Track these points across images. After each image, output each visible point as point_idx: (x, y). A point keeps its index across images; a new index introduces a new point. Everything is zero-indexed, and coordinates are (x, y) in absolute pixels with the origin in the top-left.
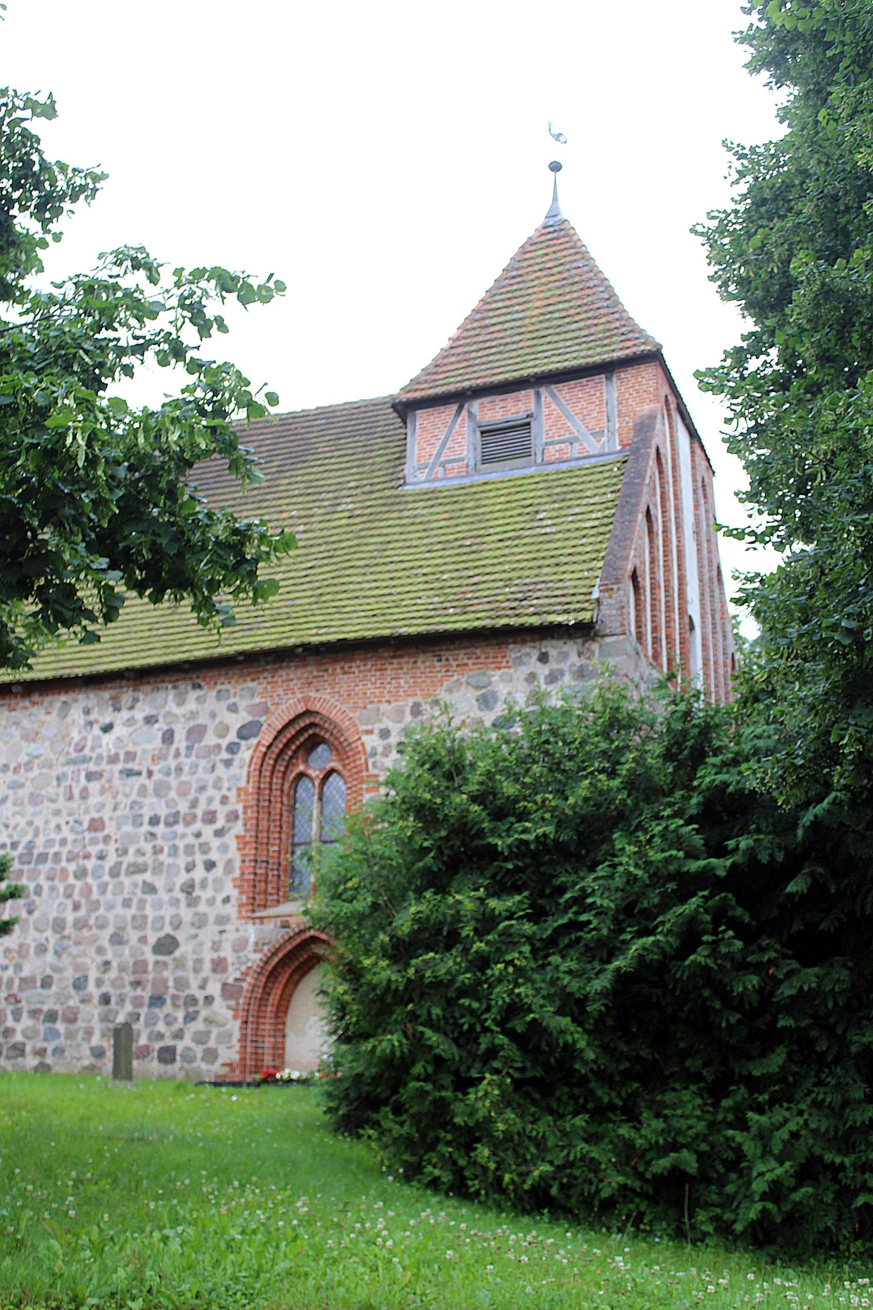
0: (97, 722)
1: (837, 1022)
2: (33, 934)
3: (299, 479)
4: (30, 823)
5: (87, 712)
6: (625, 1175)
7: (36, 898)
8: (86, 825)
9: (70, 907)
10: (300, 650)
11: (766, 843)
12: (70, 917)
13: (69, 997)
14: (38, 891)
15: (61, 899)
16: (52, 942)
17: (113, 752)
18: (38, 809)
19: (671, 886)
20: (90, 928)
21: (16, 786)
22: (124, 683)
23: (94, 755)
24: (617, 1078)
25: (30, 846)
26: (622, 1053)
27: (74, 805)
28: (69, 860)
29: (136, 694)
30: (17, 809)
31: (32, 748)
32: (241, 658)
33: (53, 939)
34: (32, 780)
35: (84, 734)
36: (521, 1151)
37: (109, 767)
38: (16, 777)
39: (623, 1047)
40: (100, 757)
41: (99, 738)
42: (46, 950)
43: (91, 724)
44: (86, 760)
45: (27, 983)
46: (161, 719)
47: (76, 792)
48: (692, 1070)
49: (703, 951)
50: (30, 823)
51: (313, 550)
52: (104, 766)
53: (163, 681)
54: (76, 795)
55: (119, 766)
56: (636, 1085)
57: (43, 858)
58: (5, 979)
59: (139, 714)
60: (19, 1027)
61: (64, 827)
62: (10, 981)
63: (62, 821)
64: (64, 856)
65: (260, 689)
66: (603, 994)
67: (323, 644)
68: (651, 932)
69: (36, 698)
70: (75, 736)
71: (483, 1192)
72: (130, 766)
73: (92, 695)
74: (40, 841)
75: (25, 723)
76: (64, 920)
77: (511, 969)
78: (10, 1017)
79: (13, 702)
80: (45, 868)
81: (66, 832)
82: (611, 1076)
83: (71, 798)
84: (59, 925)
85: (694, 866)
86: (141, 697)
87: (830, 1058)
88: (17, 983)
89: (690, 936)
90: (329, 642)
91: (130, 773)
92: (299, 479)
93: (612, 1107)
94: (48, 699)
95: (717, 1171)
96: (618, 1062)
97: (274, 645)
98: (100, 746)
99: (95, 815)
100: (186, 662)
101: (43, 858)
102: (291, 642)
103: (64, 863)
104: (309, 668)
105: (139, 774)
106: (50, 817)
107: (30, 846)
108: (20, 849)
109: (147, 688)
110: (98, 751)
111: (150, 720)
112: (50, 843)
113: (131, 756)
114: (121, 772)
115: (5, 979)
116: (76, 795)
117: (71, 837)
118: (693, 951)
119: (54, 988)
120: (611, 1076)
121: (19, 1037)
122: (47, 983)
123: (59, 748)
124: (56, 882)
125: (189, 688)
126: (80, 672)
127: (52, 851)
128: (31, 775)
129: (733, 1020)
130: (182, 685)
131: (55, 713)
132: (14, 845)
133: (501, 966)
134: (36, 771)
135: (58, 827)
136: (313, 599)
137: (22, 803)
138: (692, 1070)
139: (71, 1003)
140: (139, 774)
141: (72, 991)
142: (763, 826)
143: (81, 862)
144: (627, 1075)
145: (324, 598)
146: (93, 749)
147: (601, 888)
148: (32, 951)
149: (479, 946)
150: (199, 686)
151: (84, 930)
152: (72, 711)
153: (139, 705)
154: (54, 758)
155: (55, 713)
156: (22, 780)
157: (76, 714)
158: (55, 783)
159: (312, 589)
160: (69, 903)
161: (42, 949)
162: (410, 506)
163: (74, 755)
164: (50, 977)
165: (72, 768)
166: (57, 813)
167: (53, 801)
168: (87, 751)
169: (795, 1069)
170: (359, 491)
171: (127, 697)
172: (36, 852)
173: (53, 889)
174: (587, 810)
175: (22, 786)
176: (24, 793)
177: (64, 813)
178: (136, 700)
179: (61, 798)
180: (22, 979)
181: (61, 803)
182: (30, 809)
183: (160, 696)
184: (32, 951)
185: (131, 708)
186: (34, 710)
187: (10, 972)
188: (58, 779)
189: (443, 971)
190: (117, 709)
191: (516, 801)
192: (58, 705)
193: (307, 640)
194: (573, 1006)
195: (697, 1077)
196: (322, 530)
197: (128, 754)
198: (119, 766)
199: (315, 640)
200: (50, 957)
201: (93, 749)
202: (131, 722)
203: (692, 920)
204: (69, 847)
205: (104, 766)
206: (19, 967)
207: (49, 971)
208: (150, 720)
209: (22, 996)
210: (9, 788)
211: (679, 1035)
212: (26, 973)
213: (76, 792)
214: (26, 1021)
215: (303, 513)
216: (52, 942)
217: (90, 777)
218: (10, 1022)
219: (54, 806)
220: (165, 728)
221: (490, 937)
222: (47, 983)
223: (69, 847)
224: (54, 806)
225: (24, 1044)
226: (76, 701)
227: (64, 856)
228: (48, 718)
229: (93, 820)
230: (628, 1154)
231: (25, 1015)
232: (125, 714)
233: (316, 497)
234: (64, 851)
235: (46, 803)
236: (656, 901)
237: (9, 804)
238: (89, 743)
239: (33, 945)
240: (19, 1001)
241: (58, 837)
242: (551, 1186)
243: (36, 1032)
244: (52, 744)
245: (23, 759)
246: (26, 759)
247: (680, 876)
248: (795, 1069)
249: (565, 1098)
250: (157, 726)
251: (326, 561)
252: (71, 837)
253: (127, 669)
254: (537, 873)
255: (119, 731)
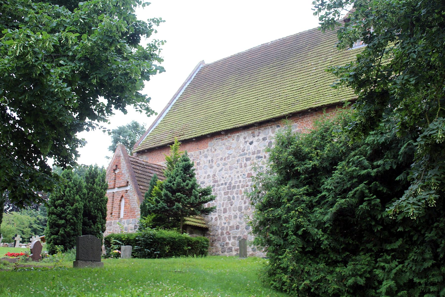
0: (248, 141)
1: (422, 229)
2: (233, 212)
3: (315, 51)
4: (230, 176)
5: (245, 138)
6: (340, 285)
7: (233, 200)
8: (246, 176)
9: (243, 203)
10: (310, 110)
11: (390, 162)
12: (243, 206)
13: (244, 232)
14: (233, 198)
15: (240, 200)
16: (238, 214)
17: (254, 150)
18: (232, 171)
19: (355, 180)
20: (250, 209)
21: (225, 164)
22: (255, 128)
23: (248, 152)
24: (340, 251)
25: (230, 183)
26: (341, 242)
27: (242, 169)
28: (242, 187)
29: (259, 131)
30: (226, 172)
31: (229, 152)
32: (291, 115)
33: (239, 213)
34: (230, 162)
35: (244, 146)
36: (302, 276)
37: (253, 156)
38: (225, 162)
39: (342, 239)
40: (249, 153)
41: (249, 146)
42: (237, 217)
43: (246, 142)
44: (245, 154)
45: (232, 227)
46: (267, 138)
47: (243, 165)
48: (369, 247)
49: (365, 204)
50: (230, 176)
51: (318, 75)
52: (251, 156)
53: (267, 126)
54: (243, 166)
55: (255, 156)
56: (348, 253)
57: (234, 187)
58: (225, 227)
59: (261, 138)
60: (230, 242)
61: (240, 177)
62: (227, 227)
63: (239, 175)
64: (240, 186)
65: (298, 125)
66: (329, 220)
67: (317, 107)
68: (345, 198)
69: (229, 135)
70: (242, 146)
71: (288, 290)
72: (259, 155)
73: (246, 133)
74: (233, 182)
75: (227, 144)
76: (241, 207)
77: (297, 213)
78: (227, 239)
79: (223, 137)
80: (235, 190)
81: (241, 178)
82: (339, 250)
83: (241, 167)
84: (240, 209)
85: (364, 172)
86: (261, 132)
87: (419, 242)
88: (229, 228)
89: (362, 198)
90: (319, 106)
91: (259, 157)
92: (315, 51)
93: (339, 262)
94: (233, 135)
95: (375, 285)
96: (341, 245)
97: (300, 109)
98: (249, 149)
99: (249, 172)
100: (273, 118)
101: (234, 187)
102: (306, 108)
103: (241, 189)
104: (314, 116)
105: (262, 157)
106: (236, 174)
107: (230, 183)
108: (227, 185)
109: (263, 128)
110: (249, 151)
111: (264, 139)
112: (236, 182)
113: (259, 152)
114: (256, 157)
115: (225, 227)
116: (243, 166)
117: (242, 180)
118: (362, 204)
119: (240, 229)
120: (339, 250)
121: (230, 246)
122: (237, 228)
123: (237, 151)
124: (239, 195)
125: (276, 127)
126: (241, 125)
127: (237, 185)
128: (229, 160)
129: (379, 229)
130: (273, 126)
131: (235, 140)
132: (226, 184)
133: (294, 212)
134: (231, 159)
135: (238, 177)
136: (316, 92)
137: (227, 170)
138: (369, 247)
139: (245, 234)
140: (262, 157)
141: (245, 230)
142: (389, 156)
143: (246, 188)
144: (345, 250)
145: (319, 92)
146: (247, 150)
147: (328, 183)
148: (233, 217)
149: (288, 205)
150: (279, 126)
151: (248, 210)
152: (240, 138)
153: (260, 135)
154: (236, 154)
155: (235, 140)
156: (227, 162)
157: (241, 139)
158: (236, 162)
159: (316, 89)
160: (243, 201)
161: (235, 217)
162: (351, 55)
163: (242, 153)
164: (238, 226)
165: (241, 157)
166: (238, 172)
167: (236, 168)
168: (245, 151)
169: (407, 247)
170: (334, 52)
171: (256, 132)
172: (232, 185)
173: (238, 197)
174: (331, 155)
175: (227, 164)
176: (227, 166)
177: (240, 172)
178: (259, 133)
179: (239, 167)
180: (230, 227)
181: (239, 169)
182: (230, 171)
183: (267, 131)
184: (233, 217)
185: (258, 136)
186: (229, 139)
187: (227, 225)
188: (237, 161)
189: (277, 214)
190: (254, 137)
191: (309, 153)
192: (236, 137)
193: (311, 107)
194: (320, 225)
195: (369, 251)
196: (321, 68)
197: (258, 151)
198: (255, 156)
199: (314, 106)
200: (238, 219)
201: (247, 150)
202: (258, 140)
203: (362, 192)
204: (242, 183)
205: (251, 156)
206: (229, 223)
207: (238, 224)
208: (264, 139)
209: (231, 232)
210: (223, 165)
211: (364, 235)
212: (231, 225)
213: (243, 165)
214: (232, 240)
215: (315, 63)
216: (238, 214)
217: (247, 159)
218: (227, 241)
219: (237, 170)
220: (269, 141)
221: (291, 202)
222: (237, 228)
223: (242, 183)
224: (237, 170)
225: (232, 247)
226: (241, 135)
227: (240, 186)
228: (233, 141)
229: (248, 174)
230: (342, 279)
231: (232, 238)
232: (256, 138)
233: (320, 57)
234: (240, 184)
235: (234, 169)
236: (349, 186)
237: (223, 171)
238: (246, 148)
239: (233, 215)
240: (230, 234)
241: (238, 180)
242: (312, 289)
243: (235, 243)
244: (235, 149)
245: (227, 155)
246: (228, 155)
247: (359, 176)
248: (407, 247)
249: (322, 258)
250: (266, 141)
251: (321, 79)
252: (242, 180)
253: (255, 123)
254: (313, 178)
255: (255, 143)
